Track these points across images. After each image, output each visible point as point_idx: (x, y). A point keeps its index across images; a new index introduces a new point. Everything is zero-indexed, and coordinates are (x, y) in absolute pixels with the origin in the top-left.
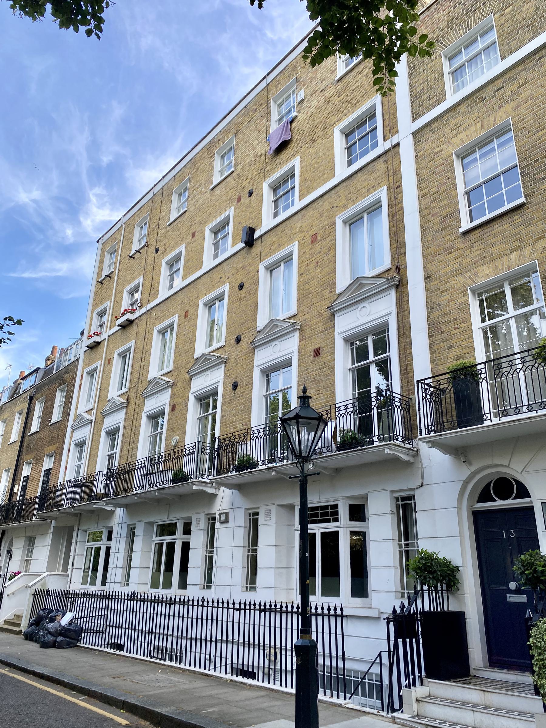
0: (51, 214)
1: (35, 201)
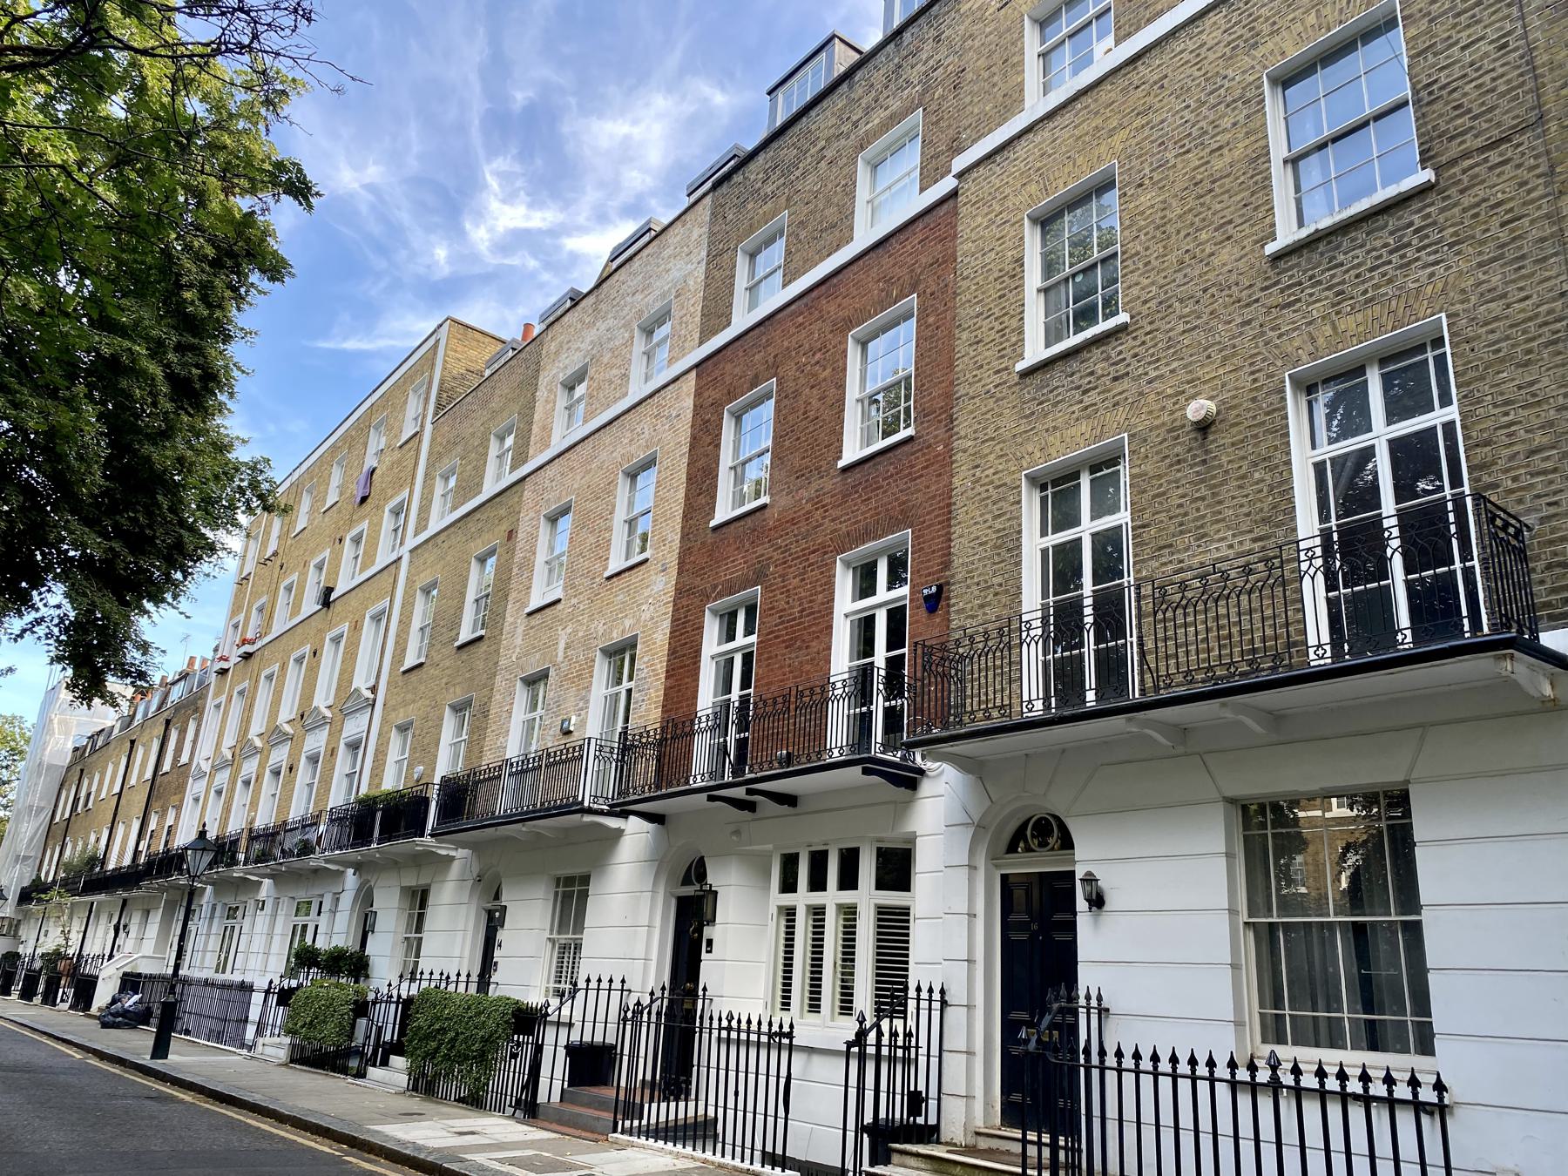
0: (404, 217)
1: (370, 188)
